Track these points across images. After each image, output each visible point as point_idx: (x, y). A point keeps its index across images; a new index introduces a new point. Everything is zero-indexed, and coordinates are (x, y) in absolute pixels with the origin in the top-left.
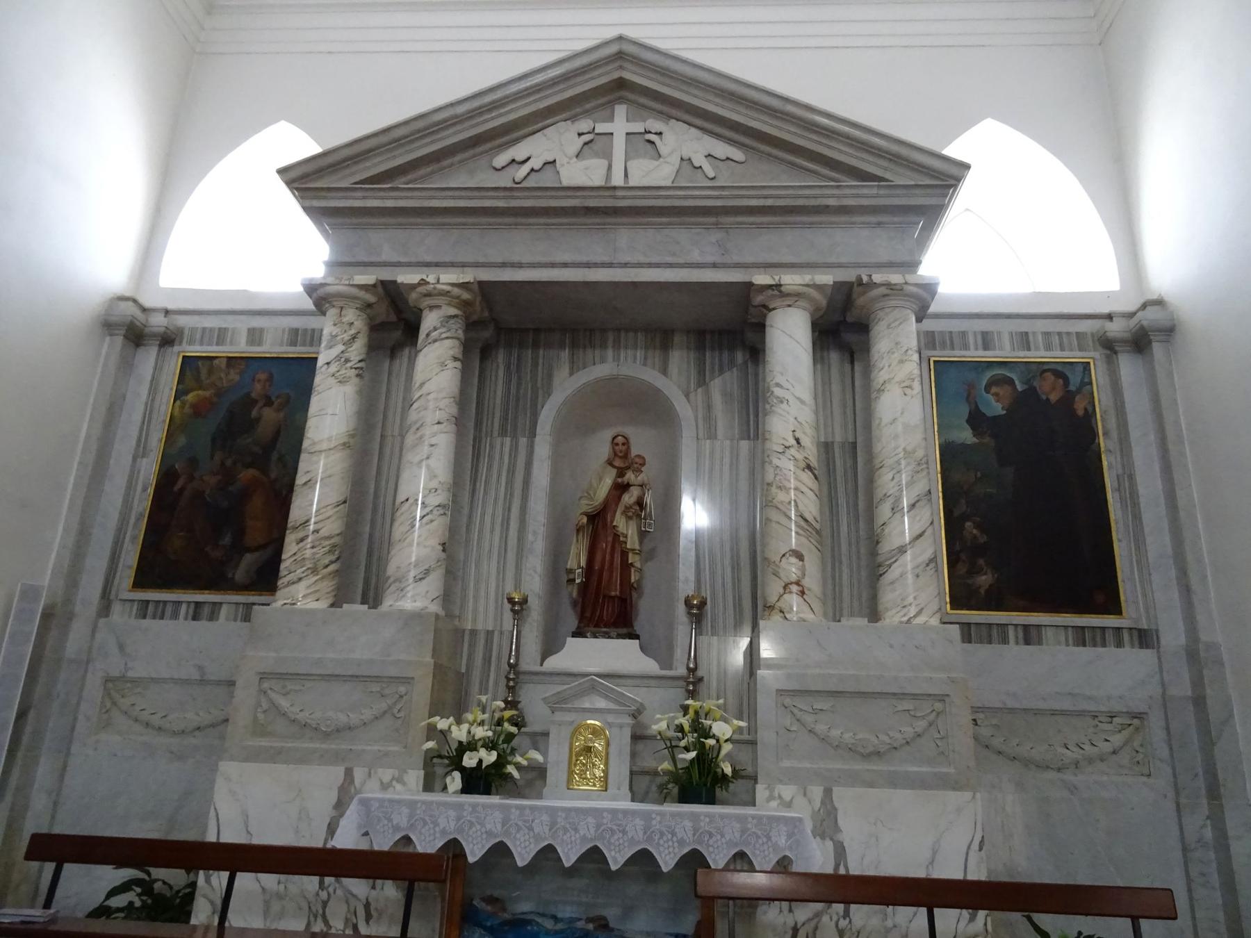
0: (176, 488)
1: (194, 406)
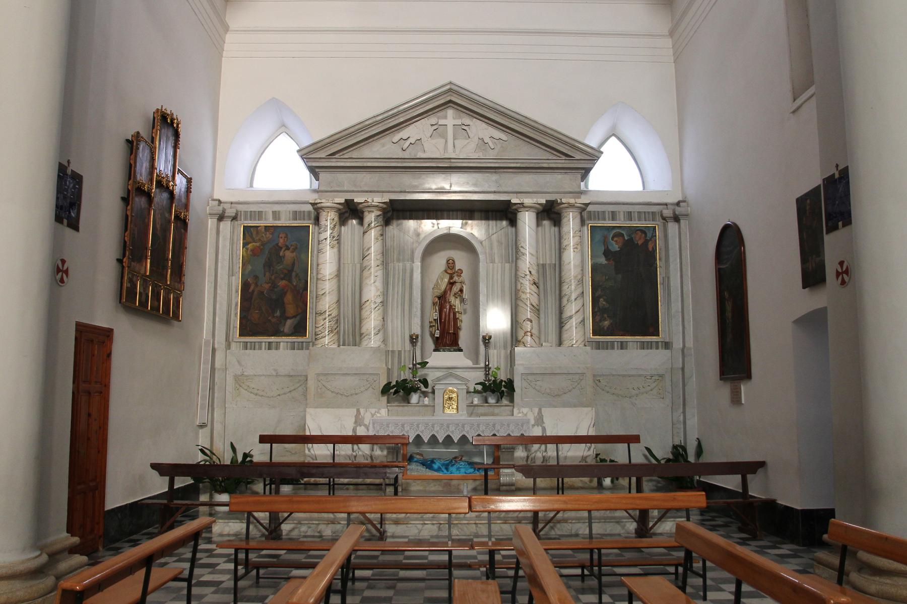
0: (250, 290)
1: (252, 251)
